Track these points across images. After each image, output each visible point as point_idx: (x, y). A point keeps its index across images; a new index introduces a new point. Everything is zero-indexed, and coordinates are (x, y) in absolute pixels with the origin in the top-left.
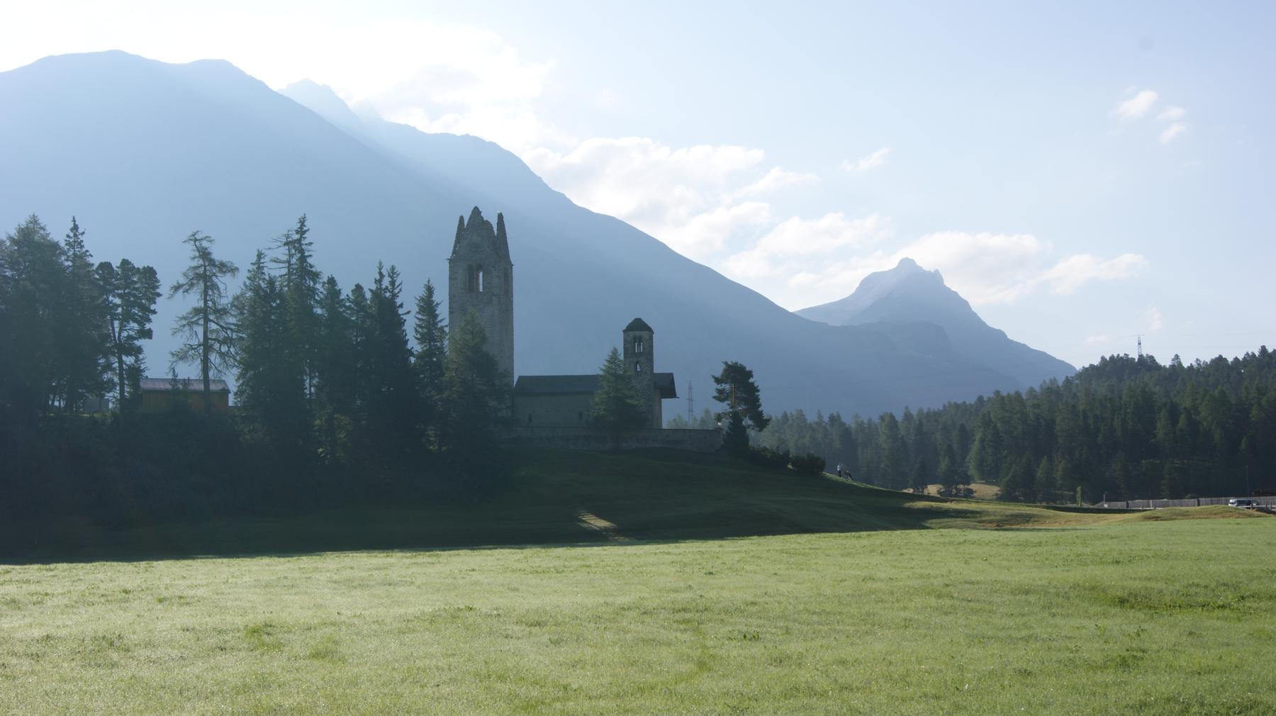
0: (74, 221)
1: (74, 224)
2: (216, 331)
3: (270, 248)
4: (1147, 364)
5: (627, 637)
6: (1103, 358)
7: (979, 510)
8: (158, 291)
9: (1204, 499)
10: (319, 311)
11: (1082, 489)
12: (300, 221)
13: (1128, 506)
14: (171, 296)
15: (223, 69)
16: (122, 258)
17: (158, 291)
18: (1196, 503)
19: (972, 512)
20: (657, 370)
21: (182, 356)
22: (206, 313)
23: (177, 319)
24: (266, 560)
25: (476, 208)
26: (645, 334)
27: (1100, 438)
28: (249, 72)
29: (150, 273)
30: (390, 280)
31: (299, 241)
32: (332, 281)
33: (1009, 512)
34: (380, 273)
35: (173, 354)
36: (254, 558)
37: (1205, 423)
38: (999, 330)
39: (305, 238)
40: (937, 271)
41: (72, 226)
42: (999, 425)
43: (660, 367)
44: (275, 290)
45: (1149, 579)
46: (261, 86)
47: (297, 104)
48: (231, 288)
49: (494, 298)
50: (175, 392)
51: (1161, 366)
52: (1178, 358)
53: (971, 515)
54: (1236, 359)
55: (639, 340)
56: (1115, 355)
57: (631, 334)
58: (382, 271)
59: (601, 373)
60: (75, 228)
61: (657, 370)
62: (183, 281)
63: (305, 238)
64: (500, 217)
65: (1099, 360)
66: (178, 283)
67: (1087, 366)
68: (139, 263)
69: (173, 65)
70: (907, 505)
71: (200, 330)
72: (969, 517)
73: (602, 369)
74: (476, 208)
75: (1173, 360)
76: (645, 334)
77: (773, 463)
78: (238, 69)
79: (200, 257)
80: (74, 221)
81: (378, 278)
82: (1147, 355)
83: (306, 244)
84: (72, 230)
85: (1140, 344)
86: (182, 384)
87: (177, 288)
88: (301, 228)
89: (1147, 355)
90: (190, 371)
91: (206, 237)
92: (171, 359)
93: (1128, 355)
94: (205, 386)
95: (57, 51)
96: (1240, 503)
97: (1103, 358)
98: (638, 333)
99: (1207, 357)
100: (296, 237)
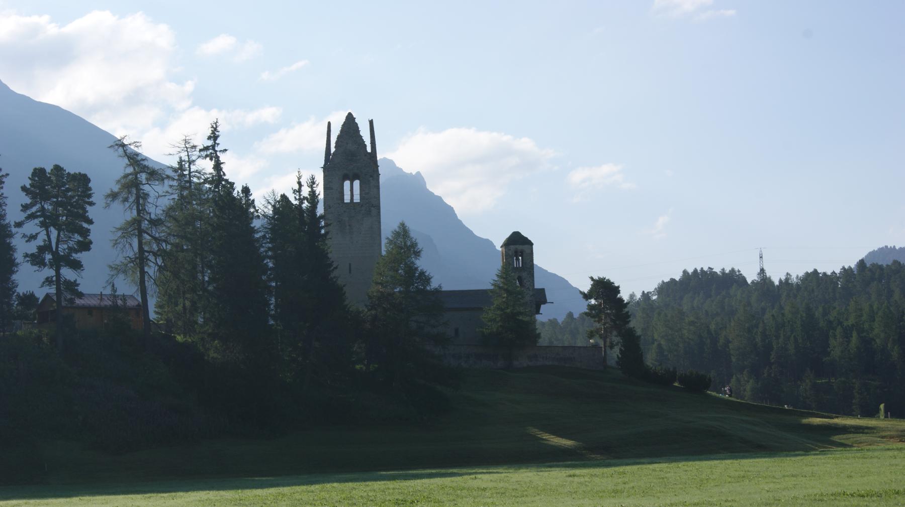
2: (149, 243)
3: (170, 154)
4: (733, 279)
6: (685, 272)
7: (870, 426)
11: (885, 407)
12: (212, 127)
16: (418, 170)
21: (118, 269)
22: (136, 227)
23: (114, 230)
26: (525, 247)
27: (772, 356)
29: (82, 180)
30: (310, 189)
31: (213, 147)
34: (300, 183)
35: (110, 267)
36: (520, 468)
37: (878, 341)
38: (487, 240)
39: (218, 144)
40: (418, 173)
42: (663, 342)
43: (538, 285)
44: (308, 198)
45: (863, 496)
49: (372, 208)
50: (115, 308)
51: (669, 281)
53: (869, 431)
54: (834, 272)
55: (517, 254)
57: (513, 247)
58: (301, 180)
62: (116, 189)
63: (218, 144)
65: (681, 274)
66: (112, 191)
67: (667, 280)
71: (135, 242)
72: (867, 433)
73: (493, 285)
77: (663, 380)
81: (296, 187)
83: (220, 151)
85: (761, 257)
86: (121, 299)
87: (114, 196)
88: (213, 133)
90: (127, 287)
91: (135, 142)
92: (112, 273)
93: (712, 269)
97: (685, 272)
98: (520, 247)
99: (797, 271)
100: (210, 143)
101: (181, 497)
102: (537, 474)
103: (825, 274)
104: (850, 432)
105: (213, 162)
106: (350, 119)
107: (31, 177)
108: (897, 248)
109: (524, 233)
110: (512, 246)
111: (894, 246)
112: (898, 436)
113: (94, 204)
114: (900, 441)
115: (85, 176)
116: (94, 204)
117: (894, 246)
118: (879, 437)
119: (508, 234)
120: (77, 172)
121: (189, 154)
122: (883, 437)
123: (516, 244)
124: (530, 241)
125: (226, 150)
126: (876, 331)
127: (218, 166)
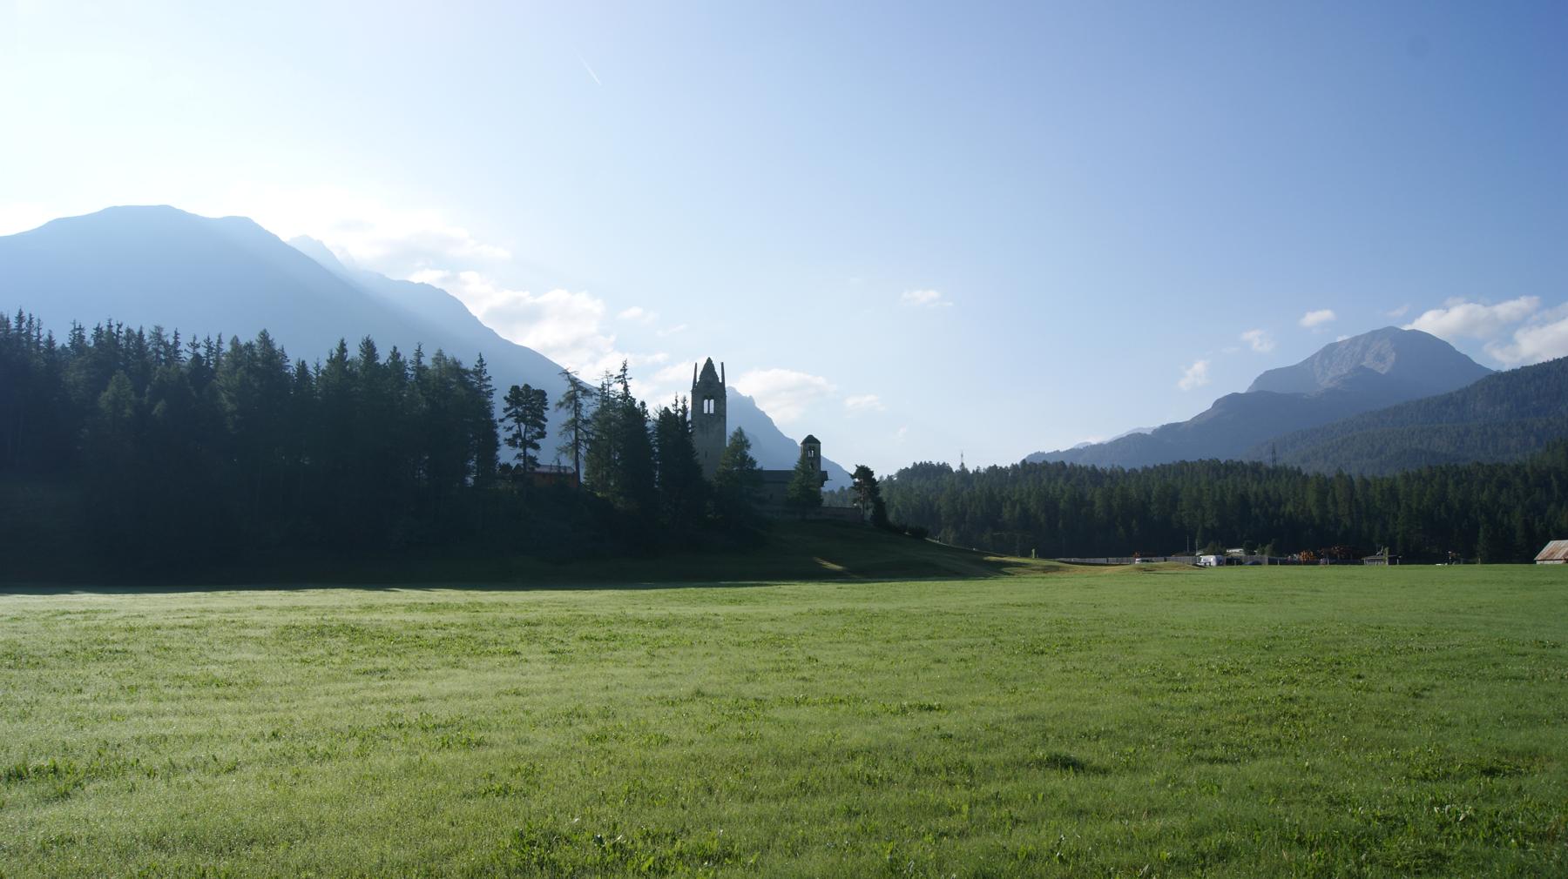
0: (480, 355)
4: (944, 469)
8: (547, 406)
14: (557, 410)
15: (246, 222)
17: (547, 406)
20: (822, 469)
21: (563, 450)
22: (574, 424)
28: (266, 227)
29: (542, 394)
33: (52, 608)
41: (479, 358)
42: (899, 507)
46: (275, 239)
47: (308, 258)
48: (590, 407)
50: (559, 474)
56: (918, 463)
57: (808, 444)
59: (794, 469)
60: (481, 360)
61: (822, 469)
68: (535, 387)
69: (203, 218)
70: (986, 558)
71: (573, 434)
78: (257, 225)
79: (572, 385)
80: (480, 355)
81: (675, 403)
82: (1072, 464)
84: (478, 362)
89: (1072, 464)
90: (567, 462)
95: (120, 203)
96: (1143, 561)
98: (812, 445)
100: (622, 373)
103: (1001, 468)
106: (709, 362)
112: (1042, 570)
126: (1031, 504)
127: (626, 388)
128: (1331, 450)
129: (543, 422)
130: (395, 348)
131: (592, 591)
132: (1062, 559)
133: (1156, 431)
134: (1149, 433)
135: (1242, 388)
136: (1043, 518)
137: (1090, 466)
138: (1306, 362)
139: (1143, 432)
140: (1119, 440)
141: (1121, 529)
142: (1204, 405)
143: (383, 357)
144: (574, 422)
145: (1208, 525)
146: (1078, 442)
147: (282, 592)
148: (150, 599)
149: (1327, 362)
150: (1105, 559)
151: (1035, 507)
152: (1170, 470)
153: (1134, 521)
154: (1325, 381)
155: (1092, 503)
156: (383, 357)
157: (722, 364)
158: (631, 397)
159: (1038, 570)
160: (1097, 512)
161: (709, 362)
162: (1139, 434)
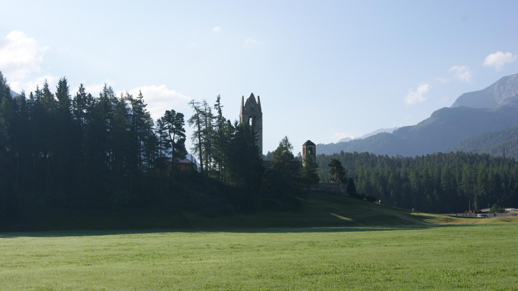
1: (140, 93)
5: (442, 260)
9: (459, 214)
10: (225, 134)
12: (218, 97)
13: (463, 215)
18: (493, 215)
19: (433, 217)
24: (179, 234)
25: (252, 93)
26: (313, 146)
29: (181, 116)
32: (229, 121)
37: (372, 184)
41: (139, 93)
52: (300, 154)
57: (308, 146)
60: (141, 94)
64: (259, 97)
65: (267, 153)
74: (252, 93)
75: (298, 154)
76: (313, 146)
88: (218, 99)
92: (191, 151)
94: (172, 160)
98: (311, 146)
101: (174, 237)
102: (381, 232)
103: (328, 156)
104: (428, 219)
105: (218, 110)
106: (252, 95)
107: (165, 114)
108: (325, 144)
109: (312, 141)
110: (308, 146)
111: (324, 144)
112: (445, 221)
113: (185, 125)
114: (446, 222)
115: (182, 114)
116: (185, 125)
117: (324, 144)
118: (439, 220)
119: (305, 141)
120: (181, 113)
121: (206, 106)
122: (440, 221)
123: (310, 145)
124: (314, 144)
125: (223, 106)
126: (372, 180)
127: (220, 112)
128: (510, 146)
129: (183, 133)
130: (82, 85)
131: (83, 237)
132: (451, 214)
133: (395, 132)
134: (391, 132)
135: (449, 105)
136: (380, 189)
137: (385, 155)
138: (488, 88)
139: (387, 132)
140: (372, 136)
141: (428, 196)
142: (425, 114)
143: (73, 93)
144: (199, 131)
145: (480, 194)
146: (339, 140)
147: (121, 235)
148: (138, 235)
149: (502, 88)
150: (456, 214)
151: (374, 182)
152: (320, 158)
153: (435, 191)
154: (501, 101)
155: (407, 180)
156: (73, 93)
157: (243, 96)
158: (223, 117)
159: (443, 221)
160: (412, 185)
161: (252, 95)
162: (385, 133)
